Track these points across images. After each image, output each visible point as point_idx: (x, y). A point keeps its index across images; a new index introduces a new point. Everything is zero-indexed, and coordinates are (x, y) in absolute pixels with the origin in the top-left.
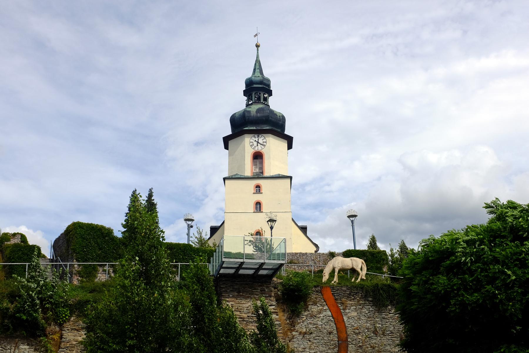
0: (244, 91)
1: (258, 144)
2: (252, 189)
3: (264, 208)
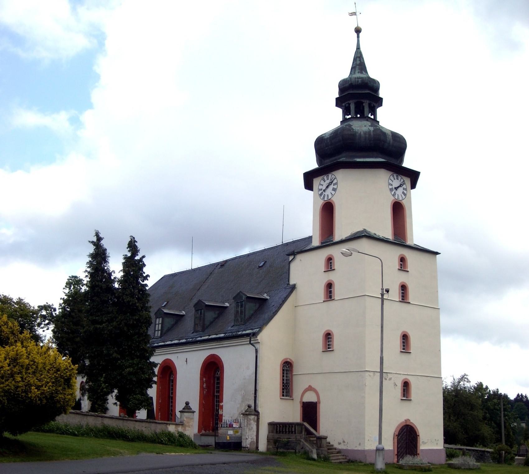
0: (337, 99)
2: (396, 263)
3: (338, 292)
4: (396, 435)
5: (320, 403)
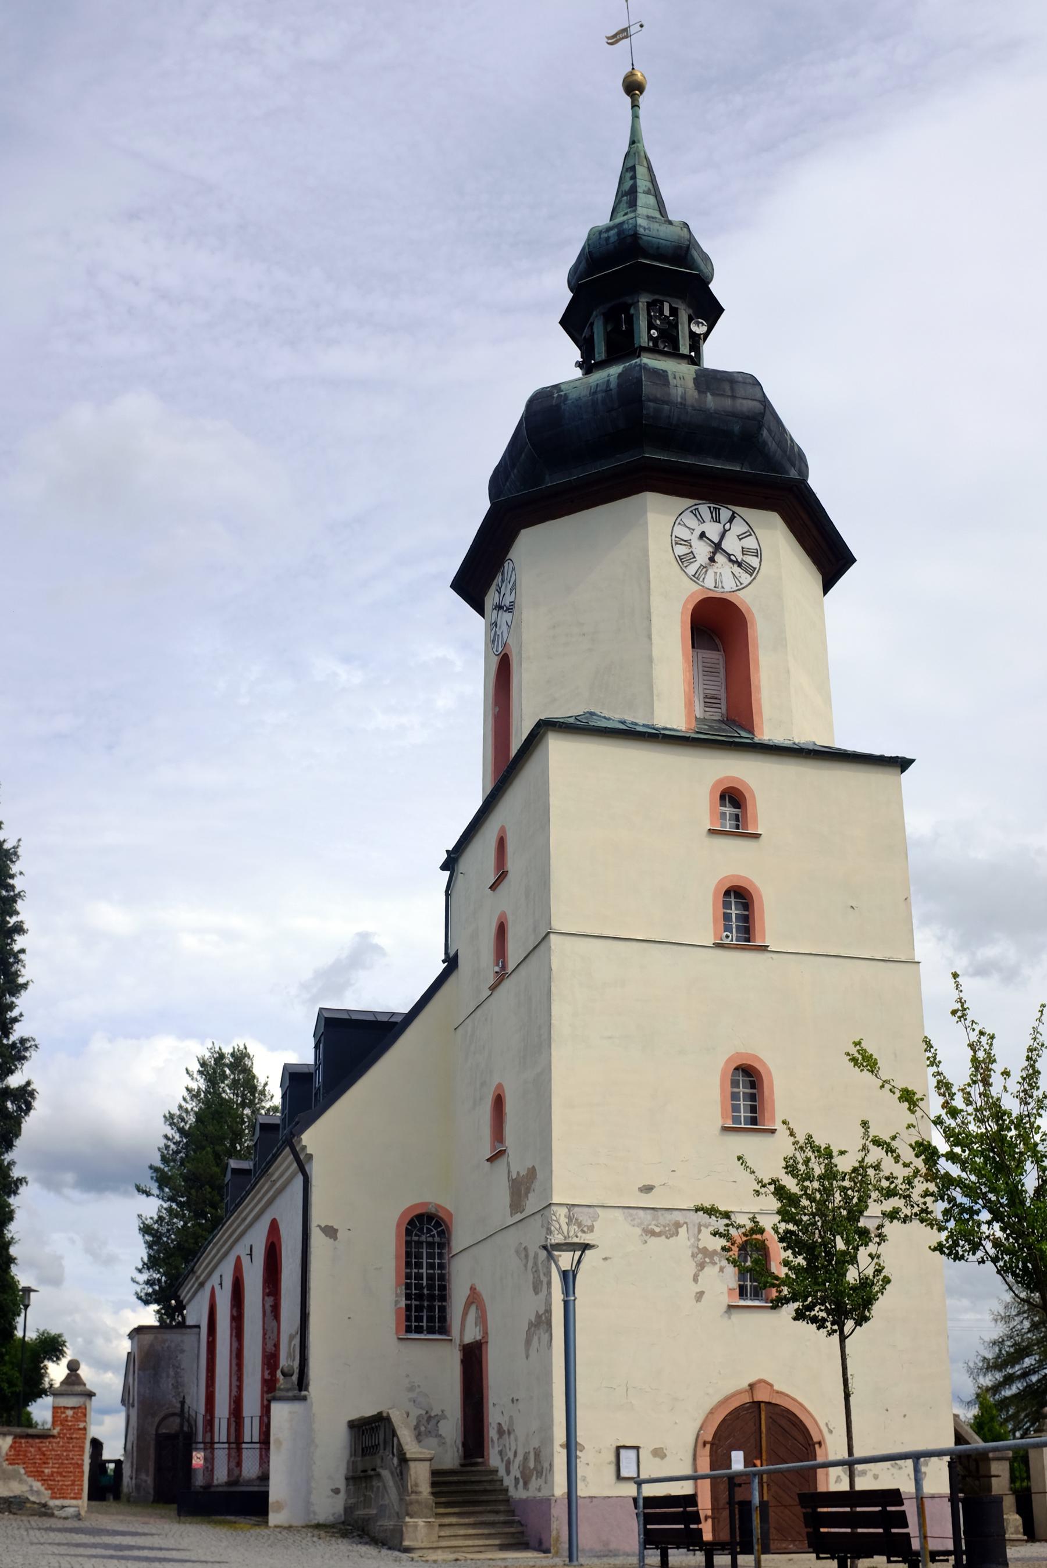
1: (714, 553)
4: (705, 1444)
5: (487, 1342)
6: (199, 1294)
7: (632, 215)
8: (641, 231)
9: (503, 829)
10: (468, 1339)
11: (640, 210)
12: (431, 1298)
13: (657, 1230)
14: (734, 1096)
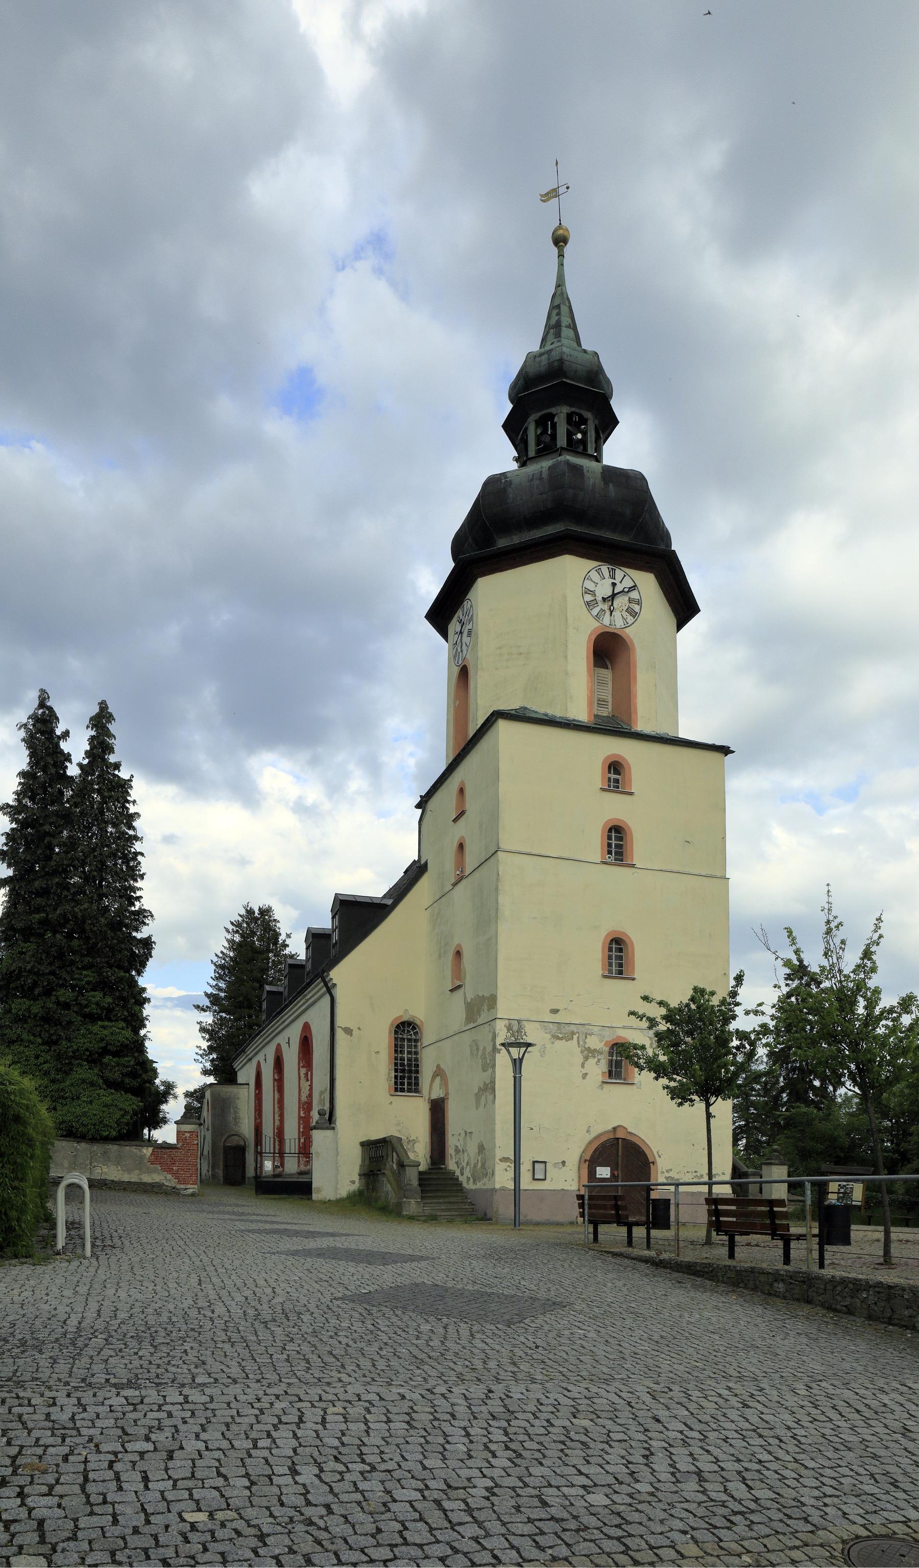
2: (596, 776)
4: (585, 1161)
6: (248, 1065)
7: (559, 344)
8: (565, 357)
9: (462, 783)
10: (434, 1096)
11: (564, 341)
12: (410, 1071)
13: (560, 1036)
14: (610, 957)
